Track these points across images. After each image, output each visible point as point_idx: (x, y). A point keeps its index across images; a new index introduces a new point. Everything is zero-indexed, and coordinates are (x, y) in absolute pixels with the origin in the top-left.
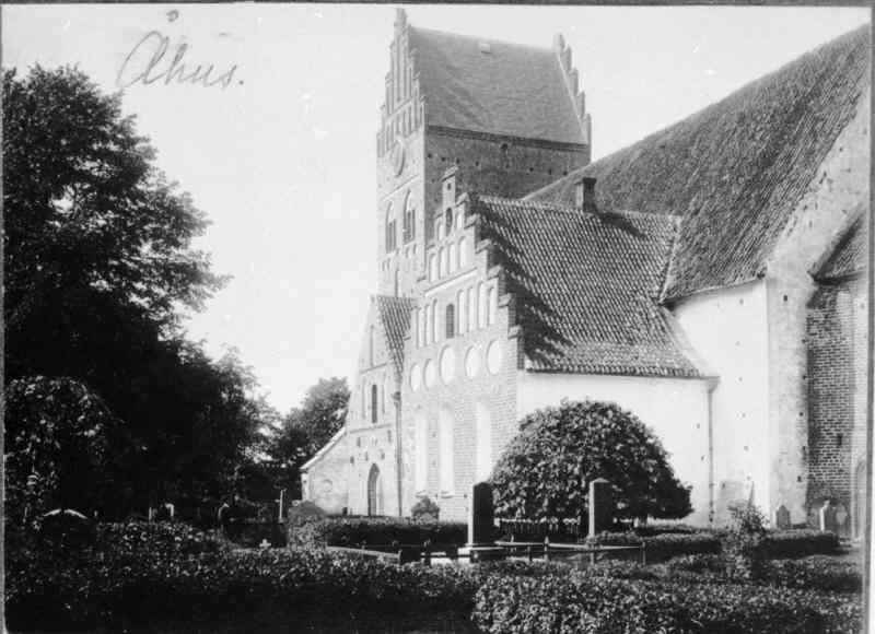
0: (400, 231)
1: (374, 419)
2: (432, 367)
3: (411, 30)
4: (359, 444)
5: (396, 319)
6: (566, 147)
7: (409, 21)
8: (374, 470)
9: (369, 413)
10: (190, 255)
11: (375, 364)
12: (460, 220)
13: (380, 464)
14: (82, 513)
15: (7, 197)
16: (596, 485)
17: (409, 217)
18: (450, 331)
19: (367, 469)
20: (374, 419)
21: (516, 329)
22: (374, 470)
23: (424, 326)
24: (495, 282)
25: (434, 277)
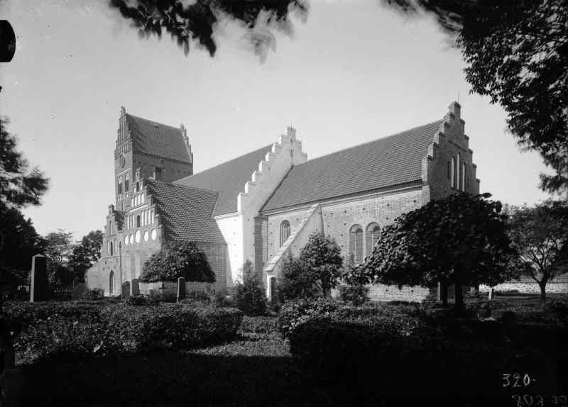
0: (124, 186)
1: (112, 254)
2: (132, 237)
3: (127, 114)
4: (106, 263)
5: (118, 217)
6: (185, 163)
7: (126, 111)
8: (112, 273)
9: (109, 252)
10: (421, 187)
11: (112, 234)
12: (141, 188)
13: (114, 271)
14: (205, 357)
15: (565, 68)
16: (180, 280)
17: (127, 183)
18: (139, 225)
19: (109, 272)
20: (112, 254)
21: (160, 226)
22: (112, 273)
23: (130, 223)
24: (154, 209)
25: (132, 205)
